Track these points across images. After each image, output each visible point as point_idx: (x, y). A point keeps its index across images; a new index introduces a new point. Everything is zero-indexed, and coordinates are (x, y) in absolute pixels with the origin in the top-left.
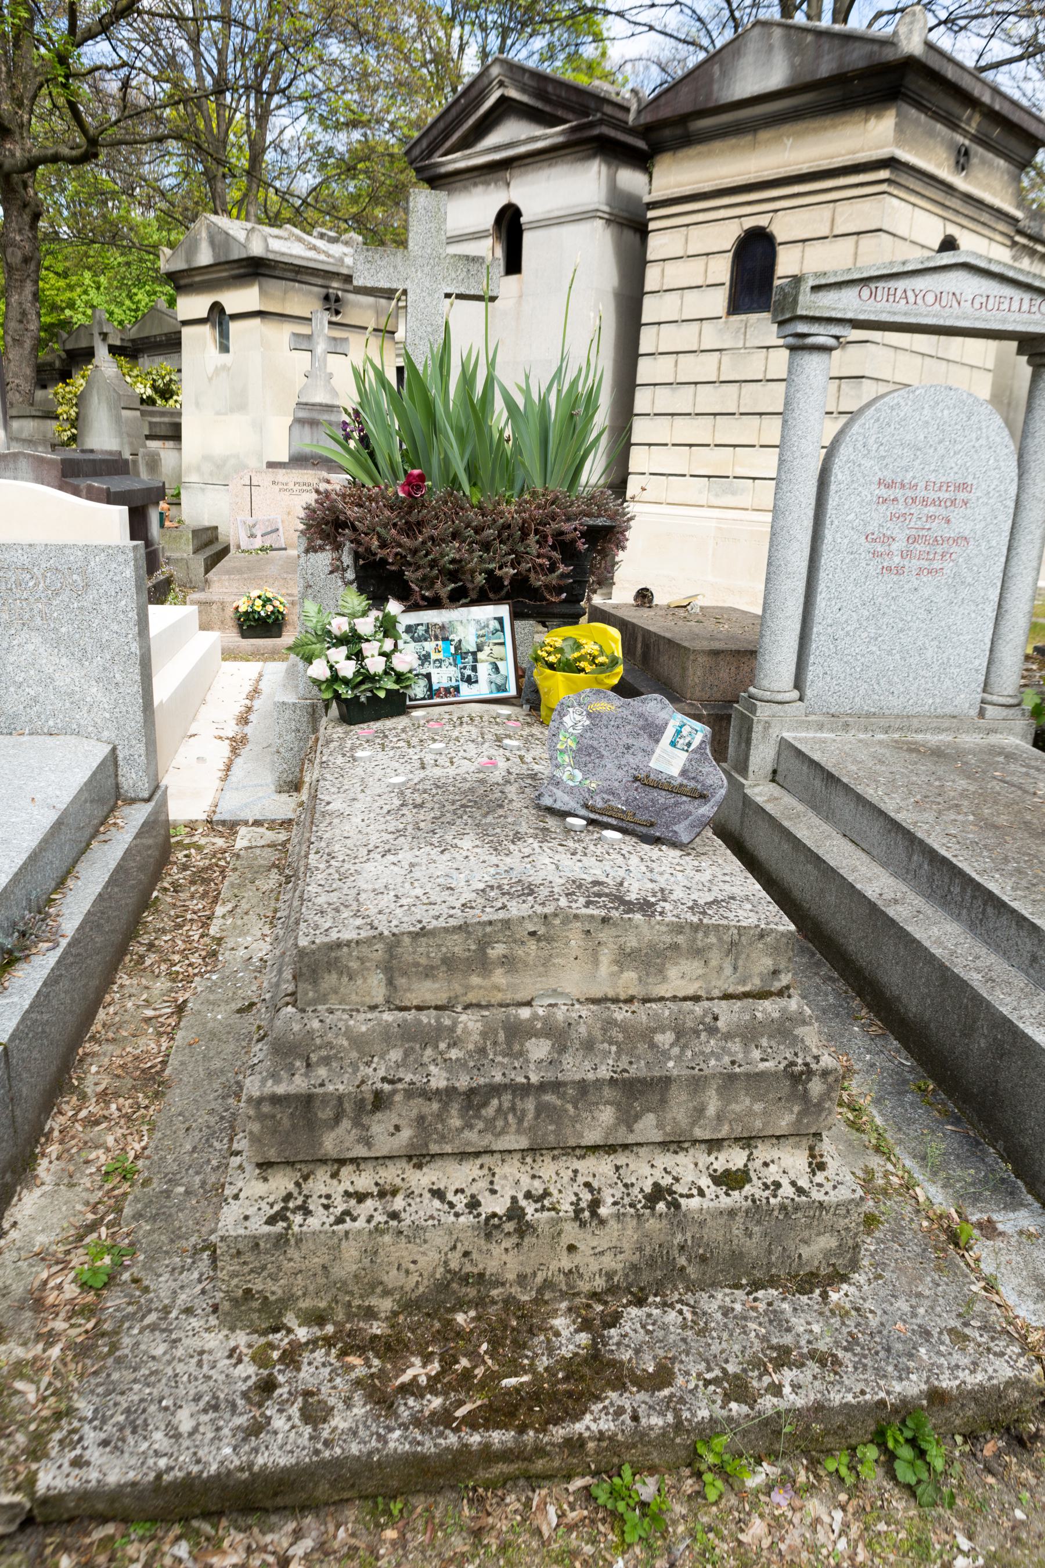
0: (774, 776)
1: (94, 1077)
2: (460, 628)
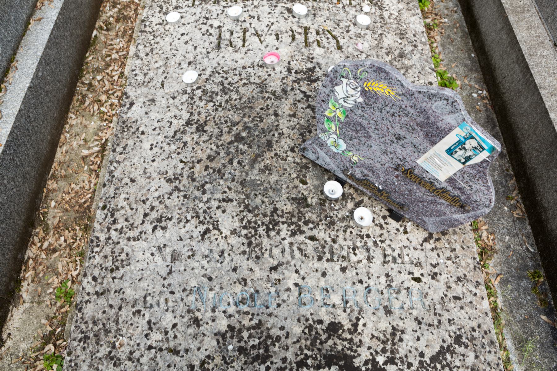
1: (53, 213)
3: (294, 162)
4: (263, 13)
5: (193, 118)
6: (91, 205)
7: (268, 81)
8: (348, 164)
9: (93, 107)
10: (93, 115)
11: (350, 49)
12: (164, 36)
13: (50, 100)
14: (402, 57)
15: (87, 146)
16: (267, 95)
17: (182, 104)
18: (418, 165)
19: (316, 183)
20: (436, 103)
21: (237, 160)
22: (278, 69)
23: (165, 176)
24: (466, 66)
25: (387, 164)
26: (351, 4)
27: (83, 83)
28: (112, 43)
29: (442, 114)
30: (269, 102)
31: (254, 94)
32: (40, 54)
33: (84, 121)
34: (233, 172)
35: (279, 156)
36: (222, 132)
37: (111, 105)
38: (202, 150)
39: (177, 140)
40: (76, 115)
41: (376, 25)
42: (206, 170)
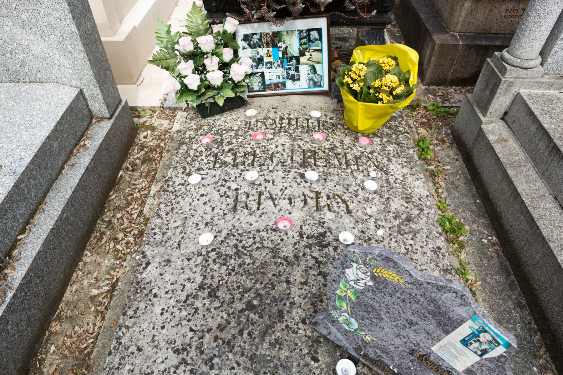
0: (504, 117)
2: (286, 38)
3: (306, 336)
4: (277, 177)
5: (207, 281)
6: (92, 351)
7: (281, 245)
8: (360, 343)
9: (109, 245)
10: (108, 253)
11: (359, 214)
12: (185, 196)
13: (69, 240)
14: (409, 221)
15: (98, 285)
16: (279, 261)
17: (196, 266)
18: (432, 352)
19: (328, 360)
20: (446, 295)
21: (247, 331)
22: (290, 234)
23: (173, 346)
24: (472, 211)
25: (401, 348)
26: (358, 169)
27: (103, 221)
28: (136, 182)
29: (452, 305)
30: (281, 268)
31: (267, 259)
32: (68, 197)
33: (99, 259)
34: (242, 344)
35: (291, 329)
36: (233, 298)
37: (127, 243)
38: (212, 318)
39: (188, 305)
40: (91, 253)
41: (383, 189)
42: (215, 341)
